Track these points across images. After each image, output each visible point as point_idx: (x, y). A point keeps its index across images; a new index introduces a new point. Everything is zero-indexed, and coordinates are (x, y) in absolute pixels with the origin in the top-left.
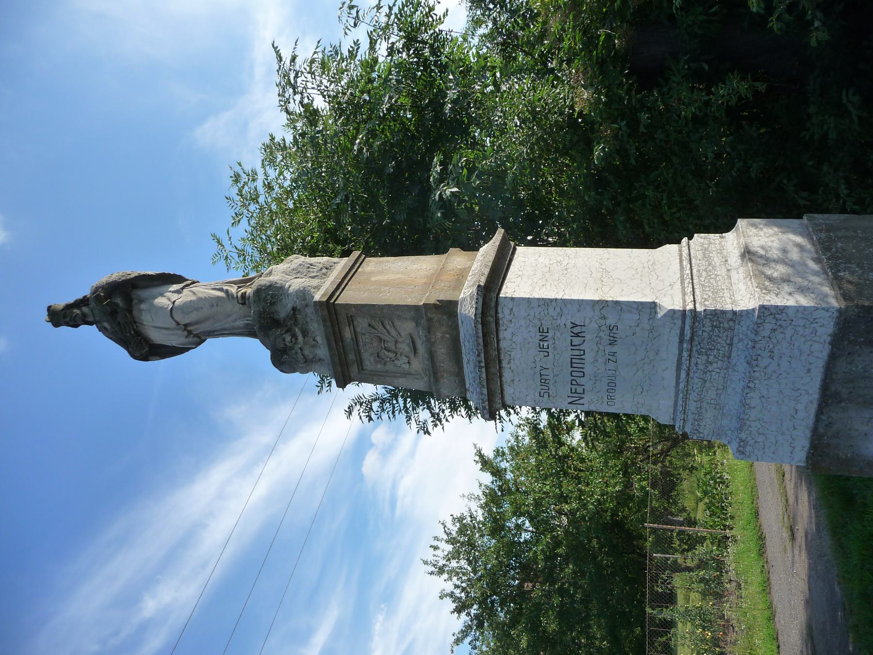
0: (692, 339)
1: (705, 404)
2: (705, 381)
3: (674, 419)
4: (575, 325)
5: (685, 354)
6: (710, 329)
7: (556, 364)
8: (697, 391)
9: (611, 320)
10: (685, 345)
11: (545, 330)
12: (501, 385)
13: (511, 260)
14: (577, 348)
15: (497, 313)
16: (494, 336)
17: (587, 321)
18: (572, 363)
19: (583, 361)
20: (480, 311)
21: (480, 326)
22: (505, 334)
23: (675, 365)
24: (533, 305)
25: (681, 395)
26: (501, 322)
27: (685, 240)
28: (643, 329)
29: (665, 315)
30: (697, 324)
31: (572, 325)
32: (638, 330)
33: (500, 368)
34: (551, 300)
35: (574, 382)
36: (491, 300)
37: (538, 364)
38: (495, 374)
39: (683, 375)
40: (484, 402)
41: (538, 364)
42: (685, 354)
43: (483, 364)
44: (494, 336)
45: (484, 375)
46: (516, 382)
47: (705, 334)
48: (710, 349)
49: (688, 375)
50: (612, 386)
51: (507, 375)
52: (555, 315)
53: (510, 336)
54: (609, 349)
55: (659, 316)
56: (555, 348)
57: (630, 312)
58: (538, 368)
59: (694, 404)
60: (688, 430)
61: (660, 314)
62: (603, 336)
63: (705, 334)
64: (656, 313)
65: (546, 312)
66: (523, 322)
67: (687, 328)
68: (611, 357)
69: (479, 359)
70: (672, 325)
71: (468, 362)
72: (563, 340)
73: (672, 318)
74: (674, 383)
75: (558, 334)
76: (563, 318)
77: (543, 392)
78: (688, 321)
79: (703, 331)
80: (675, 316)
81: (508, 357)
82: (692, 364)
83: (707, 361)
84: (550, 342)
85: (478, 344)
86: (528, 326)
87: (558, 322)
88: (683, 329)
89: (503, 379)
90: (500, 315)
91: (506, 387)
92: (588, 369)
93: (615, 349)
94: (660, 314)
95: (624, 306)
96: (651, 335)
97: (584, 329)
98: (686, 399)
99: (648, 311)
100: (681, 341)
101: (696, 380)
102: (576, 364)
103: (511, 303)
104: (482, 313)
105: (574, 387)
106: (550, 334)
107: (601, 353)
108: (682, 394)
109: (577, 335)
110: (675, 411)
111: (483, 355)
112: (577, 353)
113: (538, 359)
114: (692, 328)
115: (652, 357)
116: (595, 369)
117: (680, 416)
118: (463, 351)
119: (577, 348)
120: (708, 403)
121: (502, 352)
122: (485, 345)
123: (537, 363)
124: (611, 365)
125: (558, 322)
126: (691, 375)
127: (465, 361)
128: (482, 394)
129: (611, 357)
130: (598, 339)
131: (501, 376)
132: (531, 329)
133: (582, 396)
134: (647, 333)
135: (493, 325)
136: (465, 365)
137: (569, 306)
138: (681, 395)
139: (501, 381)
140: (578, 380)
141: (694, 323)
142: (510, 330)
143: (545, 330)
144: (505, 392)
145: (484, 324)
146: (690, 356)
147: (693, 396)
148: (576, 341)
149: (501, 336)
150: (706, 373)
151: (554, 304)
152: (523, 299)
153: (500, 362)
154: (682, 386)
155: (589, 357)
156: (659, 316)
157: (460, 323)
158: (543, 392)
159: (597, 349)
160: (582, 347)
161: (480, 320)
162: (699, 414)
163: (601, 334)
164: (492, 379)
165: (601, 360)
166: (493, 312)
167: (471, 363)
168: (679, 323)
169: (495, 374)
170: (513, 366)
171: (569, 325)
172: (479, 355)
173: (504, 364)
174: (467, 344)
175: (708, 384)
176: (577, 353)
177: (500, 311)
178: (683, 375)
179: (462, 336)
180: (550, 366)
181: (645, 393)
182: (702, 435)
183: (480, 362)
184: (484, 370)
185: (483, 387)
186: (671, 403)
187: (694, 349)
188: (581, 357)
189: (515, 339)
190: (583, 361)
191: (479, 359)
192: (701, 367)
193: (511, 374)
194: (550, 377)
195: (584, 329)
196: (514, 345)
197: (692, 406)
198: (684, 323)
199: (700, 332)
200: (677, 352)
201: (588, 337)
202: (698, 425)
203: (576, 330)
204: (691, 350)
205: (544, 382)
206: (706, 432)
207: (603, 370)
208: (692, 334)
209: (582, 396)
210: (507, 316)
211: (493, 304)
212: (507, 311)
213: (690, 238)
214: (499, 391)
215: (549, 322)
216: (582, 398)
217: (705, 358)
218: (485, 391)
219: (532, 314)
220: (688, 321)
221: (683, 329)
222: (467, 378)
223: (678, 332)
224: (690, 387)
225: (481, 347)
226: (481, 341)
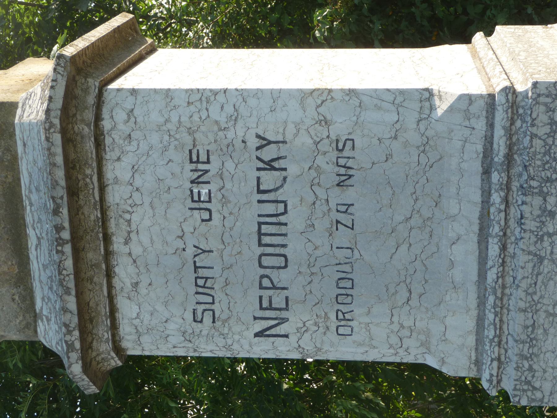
0: (509, 158)
1: (543, 315)
2: (541, 259)
3: (478, 363)
4: (265, 142)
5: (496, 198)
6: (547, 129)
7: (226, 238)
8: (524, 285)
9: (340, 128)
10: (495, 177)
11: (203, 158)
12: (111, 298)
13: (140, 59)
14: (270, 196)
15: (98, 118)
16: (91, 171)
17: (291, 129)
18: (260, 234)
19: (283, 230)
20: (59, 103)
21: (57, 138)
22: (117, 170)
23: (476, 228)
24: (176, 102)
25: (491, 299)
26: (108, 141)
27: (479, 37)
28: (406, 144)
29: (451, 109)
30: (518, 123)
31: (257, 142)
32: (396, 146)
33: (108, 254)
34: (215, 93)
35: (266, 282)
36: (86, 91)
37: (190, 242)
38: (97, 266)
39: (494, 249)
40: (69, 332)
41: (190, 242)
42: (496, 198)
43: (66, 235)
44: (91, 171)
45: (69, 263)
46: (143, 290)
47: (538, 143)
48: (548, 180)
49: (504, 248)
50: (345, 289)
51: (124, 273)
52: (222, 119)
53: (127, 176)
54: (337, 197)
55: (440, 112)
56: (225, 201)
57: (378, 108)
58: (191, 251)
59: (520, 318)
60: (508, 385)
61: (441, 108)
62: (324, 166)
63: (538, 143)
64: (432, 108)
65: (204, 115)
66: (154, 139)
67: (499, 132)
68: (342, 217)
69: (58, 220)
70: (467, 132)
71: (38, 245)
72: (238, 178)
73: (467, 115)
74: (474, 277)
75: (230, 165)
76: (240, 123)
77: (200, 308)
78: (500, 117)
79: (533, 136)
80: (474, 109)
81: (124, 226)
82: (512, 223)
83: (543, 210)
84: (213, 187)
85: (55, 184)
86: (166, 149)
87: (230, 135)
88: (489, 140)
89: (116, 282)
90: (106, 124)
91: (122, 303)
92: (295, 248)
93: (350, 195)
94: (441, 108)
95: (364, 98)
96: (423, 159)
97: (283, 150)
98: (501, 308)
99: (416, 106)
100: (486, 172)
101: (522, 258)
102: (270, 228)
103: (131, 99)
104: (65, 109)
105: (266, 294)
106: (214, 167)
107: (321, 208)
108: (493, 298)
109: (269, 165)
110: (479, 341)
111: (65, 211)
112: (270, 209)
113: (188, 229)
114: (509, 134)
115: (426, 213)
116: (310, 248)
117: (491, 351)
118: (29, 219)
119: (270, 196)
120: (549, 314)
121: (111, 214)
122: (73, 191)
123: (187, 236)
124: (343, 237)
125: (230, 135)
126: (511, 249)
127: (32, 242)
128: (65, 310)
129: (342, 217)
130: (313, 173)
131: (109, 275)
132: (171, 153)
133: (284, 314)
134: (415, 153)
135: (90, 145)
136: (33, 254)
137: (252, 102)
138: (491, 299)
139: (110, 286)
140: (274, 274)
141: (512, 123)
142: (128, 160)
143: (203, 158)
144: (118, 315)
145: (69, 140)
146: (506, 201)
147: (517, 298)
148: (269, 179)
149: (109, 175)
150: (541, 239)
151: (221, 98)
152: (155, 91)
153: (107, 239)
154: (491, 275)
155: (295, 219)
156: (440, 112)
157: (20, 149)
158: (200, 308)
159: (312, 198)
160: (280, 195)
161: (57, 122)
162: (532, 341)
163: (321, 161)
164: (91, 280)
165: (322, 225)
166: (89, 115)
167: (45, 244)
168: (481, 125)
169: (97, 266)
170: (137, 250)
171: (253, 142)
172: (56, 212)
173: (117, 244)
174: (34, 197)
175: (547, 266)
176: (270, 209)
177: (105, 113)
178: (494, 249)
179: (25, 179)
180: (214, 244)
181: (414, 302)
182: (539, 395)
183: (58, 229)
184: (68, 249)
185: (67, 292)
186: (471, 324)
187: (515, 185)
188: (278, 219)
189: (138, 182)
190: (283, 230)
191: (58, 220)
192: (531, 225)
193: (131, 269)
194: (215, 272)
195: (283, 150)
196: (136, 196)
197: (516, 323)
198: (491, 126)
199: (526, 141)
200: (477, 198)
201: (293, 170)
202: (531, 369)
203: (268, 154)
204: (508, 187)
205: (203, 285)
206: (547, 386)
207: (327, 248)
208: (510, 147)
209: (284, 314)
210: (121, 126)
211: (91, 100)
212: (120, 116)
213: (489, 33)
214: (104, 310)
215: (211, 137)
216: (284, 320)
217: (537, 201)
218: (72, 303)
219: (175, 119)
220: (500, 117)
221: (489, 140)
222: (36, 285)
223: (480, 148)
224: (509, 280)
225: (61, 192)
226: (60, 174)
